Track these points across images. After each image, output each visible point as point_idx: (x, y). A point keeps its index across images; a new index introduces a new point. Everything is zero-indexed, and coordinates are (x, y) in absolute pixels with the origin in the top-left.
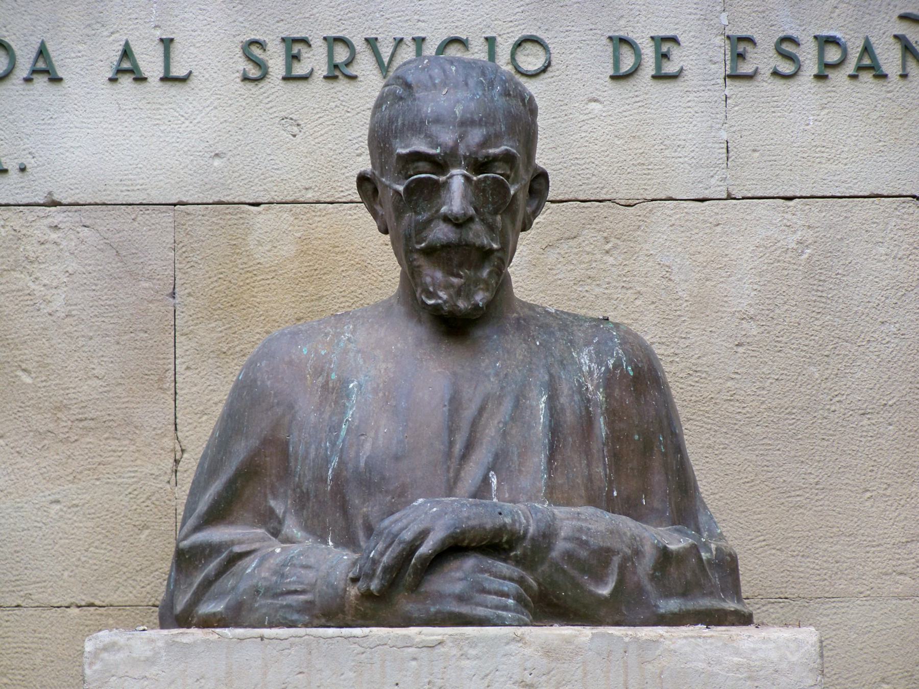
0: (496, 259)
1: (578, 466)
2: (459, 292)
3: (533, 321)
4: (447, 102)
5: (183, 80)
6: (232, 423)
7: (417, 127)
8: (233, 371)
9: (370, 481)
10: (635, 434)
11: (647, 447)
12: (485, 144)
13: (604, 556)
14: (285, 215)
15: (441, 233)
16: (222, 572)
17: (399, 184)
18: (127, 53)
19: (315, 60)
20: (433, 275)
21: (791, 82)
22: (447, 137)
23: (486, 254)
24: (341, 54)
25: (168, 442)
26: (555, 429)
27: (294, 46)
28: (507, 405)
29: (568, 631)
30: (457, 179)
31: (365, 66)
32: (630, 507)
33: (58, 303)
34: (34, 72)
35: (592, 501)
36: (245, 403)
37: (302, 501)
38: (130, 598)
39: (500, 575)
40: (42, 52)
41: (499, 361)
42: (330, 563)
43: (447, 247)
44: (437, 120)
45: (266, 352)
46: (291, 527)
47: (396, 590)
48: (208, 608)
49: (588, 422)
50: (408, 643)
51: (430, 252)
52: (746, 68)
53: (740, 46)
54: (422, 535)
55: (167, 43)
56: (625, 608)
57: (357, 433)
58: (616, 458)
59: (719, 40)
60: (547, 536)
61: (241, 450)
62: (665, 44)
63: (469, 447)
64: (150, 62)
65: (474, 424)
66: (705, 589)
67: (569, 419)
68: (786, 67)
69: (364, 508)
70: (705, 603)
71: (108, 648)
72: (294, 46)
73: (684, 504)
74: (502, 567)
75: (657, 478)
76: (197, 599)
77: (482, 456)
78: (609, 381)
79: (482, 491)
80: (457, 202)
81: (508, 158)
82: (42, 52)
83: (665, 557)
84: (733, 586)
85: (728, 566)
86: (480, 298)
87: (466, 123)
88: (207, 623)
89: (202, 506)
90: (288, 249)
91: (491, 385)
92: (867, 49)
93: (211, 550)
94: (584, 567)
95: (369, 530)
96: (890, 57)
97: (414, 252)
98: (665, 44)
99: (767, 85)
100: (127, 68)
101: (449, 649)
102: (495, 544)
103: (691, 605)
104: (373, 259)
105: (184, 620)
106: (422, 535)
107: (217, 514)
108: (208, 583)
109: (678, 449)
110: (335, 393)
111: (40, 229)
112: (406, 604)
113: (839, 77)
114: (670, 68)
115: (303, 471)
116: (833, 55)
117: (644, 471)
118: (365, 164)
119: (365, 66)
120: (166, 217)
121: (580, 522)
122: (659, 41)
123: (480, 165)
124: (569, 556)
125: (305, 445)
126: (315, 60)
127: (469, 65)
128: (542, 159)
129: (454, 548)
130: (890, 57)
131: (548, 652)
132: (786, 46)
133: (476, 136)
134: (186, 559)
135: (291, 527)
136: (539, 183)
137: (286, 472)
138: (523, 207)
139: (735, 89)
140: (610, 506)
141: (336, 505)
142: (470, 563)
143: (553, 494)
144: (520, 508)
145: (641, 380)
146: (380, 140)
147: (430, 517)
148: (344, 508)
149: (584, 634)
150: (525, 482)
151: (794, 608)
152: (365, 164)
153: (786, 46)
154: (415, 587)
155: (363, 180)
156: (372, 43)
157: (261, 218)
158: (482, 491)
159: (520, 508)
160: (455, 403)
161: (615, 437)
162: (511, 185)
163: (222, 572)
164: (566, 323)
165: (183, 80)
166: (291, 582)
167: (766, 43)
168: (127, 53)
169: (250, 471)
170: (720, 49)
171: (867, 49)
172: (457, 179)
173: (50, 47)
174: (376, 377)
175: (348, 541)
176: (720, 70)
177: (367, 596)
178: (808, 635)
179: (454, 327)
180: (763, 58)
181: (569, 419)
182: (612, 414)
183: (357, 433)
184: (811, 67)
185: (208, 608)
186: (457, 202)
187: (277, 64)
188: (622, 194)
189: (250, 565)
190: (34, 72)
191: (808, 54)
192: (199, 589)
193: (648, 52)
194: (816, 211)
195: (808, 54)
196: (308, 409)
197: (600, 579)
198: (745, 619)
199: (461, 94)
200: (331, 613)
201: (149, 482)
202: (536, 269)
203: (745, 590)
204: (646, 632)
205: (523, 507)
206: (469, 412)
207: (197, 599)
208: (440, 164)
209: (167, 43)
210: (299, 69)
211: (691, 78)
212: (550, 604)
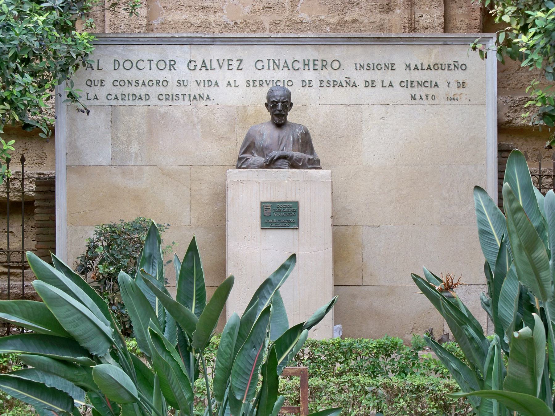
0: (285, 116)
1: (297, 146)
2: (280, 121)
3: (291, 125)
4: (278, 94)
6: (246, 139)
7: (274, 97)
8: (246, 131)
9: (267, 148)
10: (305, 142)
11: (307, 143)
12: (284, 99)
13: (300, 159)
14: (253, 107)
15: (277, 112)
16: (245, 161)
17: (271, 105)
18: (229, 82)
19: (257, 83)
20: (276, 118)
22: (278, 98)
23: (284, 115)
24: (261, 83)
26: (293, 141)
28: (287, 137)
29: (295, 170)
30: (280, 104)
31: (265, 84)
32: (304, 152)
33: (219, 120)
34: (202, 66)
35: (299, 151)
36: (248, 137)
37: (257, 151)
38: (229, 164)
39: (286, 162)
40: (216, 82)
41: (286, 131)
42: (261, 160)
43: (278, 114)
44: (277, 96)
45: (251, 129)
46: (255, 155)
47: (271, 164)
48: (243, 166)
49: (298, 140)
50: (273, 171)
51: (275, 115)
52: (322, 85)
53: (321, 82)
55: (235, 81)
56: (303, 167)
57: (265, 141)
58: (302, 145)
60: (292, 156)
61: (248, 144)
62: (310, 81)
63: (281, 143)
64: (232, 84)
65: (282, 140)
66: (314, 164)
67: (296, 139)
68: (328, 85)
69: (266, 152)
70: (315, 166)
71: (230, 172)
72: (254, 81)
73: (312, 151)
74: (286, 161)
75: (308, 148)
76: (242, 165)
77: (283, 145)
78: (301, 134)
79: (283, 150)
80: (279, 108)
81: (287, 101)
82: (216, 82)
83: (309, 159)
84: (319, 164)
85: (318, 161)
86: (283, 122)
87: (281, 96)
88: (243, 168)
89: (242, 151)
90: (253, 112)
91: (284, 134)
92: (341, 82)
93: (244, 158)
94: (298, 161)
95: (267, 155)
96: (344, 84)
97: (274, 115)
98: (310, 81)
99: (326, 88)
100: (229, 84)
101: (279, 173)
102: (285, 157)
103: (313, 166)
104: (267, 116)
105: (240, 168)
106: (274, 156)
107: (244, 152)
108: (243, 163)
109: (311, 143)
110: (262, 135)
111: (216, 109)
112: (273, 166)
113: (336, 87)
114: (311, 85)
115: (257, 147)
116: (335, 83)
117: (306, 147)
118: (266, 102)
119: (265, 84)
120: (235, 107)
121: (297, 154)
122: (309, 81)
123: (283, 102)
124: (296, 159)
125: (257, 143)
126: (257, 83)
127: (281, 87)
128: (291, 101)
129: (279, 158)
130: (344, 84)
131: (292, 173)
132: (328, 82)
133: (282, 98)
134: (240, 159)
135: (255, 155)
136: (291, 105)
137: (254, 147)
138: (289, 108)
139: (320, 88)
140: (301, 152)
141: (262, 151)
142: (281, 160)
143: (293, 150)
144: (289, 152)
145: (306, 134)
146: (268, 98)
147: (276, 153)
148: (263, 152)
149: (297, 170)
150: (289, 149)
151: (328, 166)
152: (266, 102)
153: (328, 82)
154: (274, 164)
155: (266, 104)
157: (249, 107)
158: (283, 150)
159: (289, 152)
160: (279, 137)
161: (302, 142)
162: (287, 105)
163: (245, 161)
164: (295, 125)
166: (256, 163)
167: (325, 81)
168: (229, 82)
169: (249, 146)
170: (318, 82)
171: (341, 82)
172: (280, 104)
174: (267, 133)
175: (264, 157)
176: (318, 85)
177: (267, 165)
178: (330, 171)
179: (279, 126)
180: (325, 84)
181: (296, 139)
182: (302, 138)
183: (265, 141)
184: (332, 85)
185: (243, 166)
186: (279, 108)
188: (303, 104)
189: (250, 160)
190: (202, 66)
191: (332, 83)
192: (242, 163)
193: (308, 82)
194: (333, 107)
195: (332, 83)
196: (258, 138)
197: (300, 163)
198: (321, 168)
199: (280, 92)
200: (262, 167)
201: (235, 147)
202: (291, 117)
203: (321, 164)
204: (306, 170)
205: (289, 151)
206: (281, 138)
207: (242, 165)
208: (277, 102)
209: (235, 81)
210: (255, 85)
211: (314, 86)
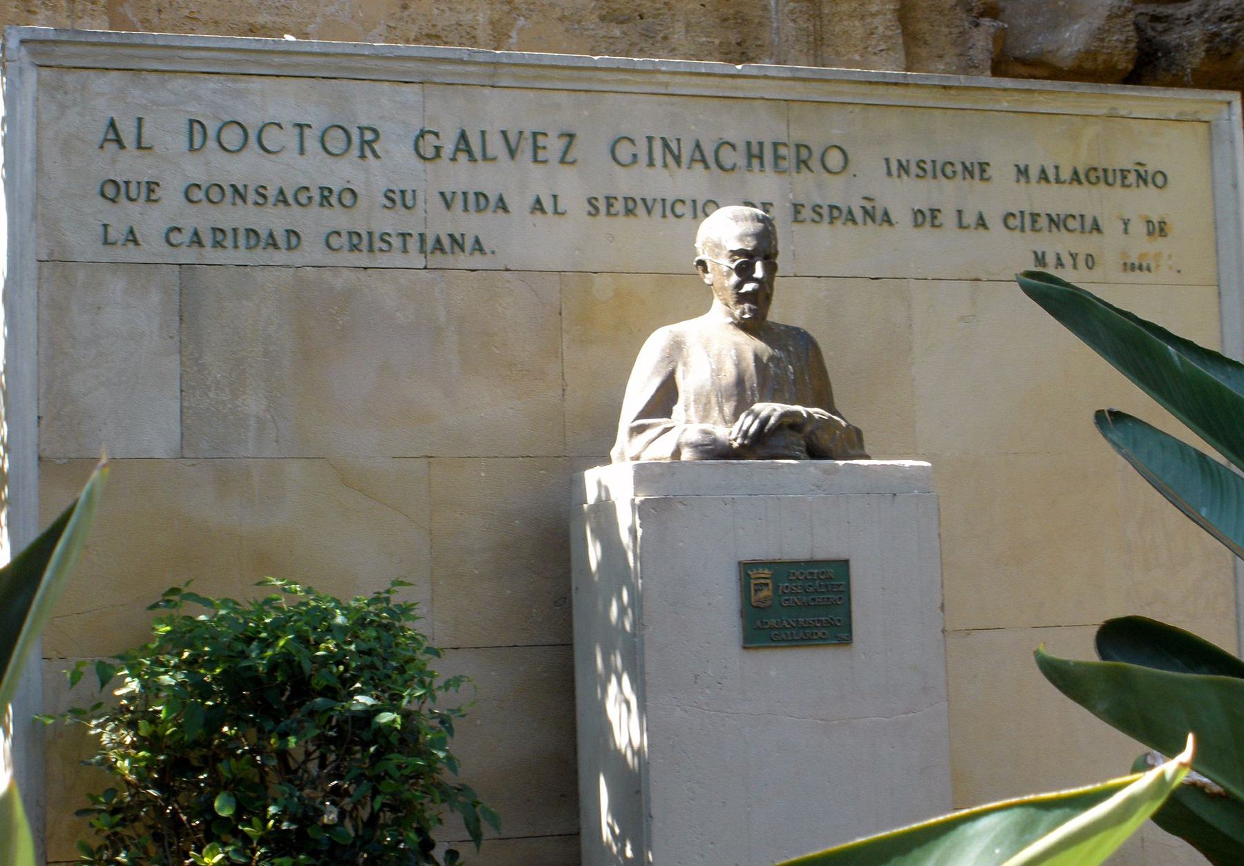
5: (563, 214)
19: (619, 206)
21: (303, 209)
25: (560, 382)
27: (610, 201)
39: (797, 440)
50: (43, 597)
54: (768, 418)
59: (788, 205)
64: (548, 204)
96: (858, 214)
99: (622, 220)
100: (538, 206)
113: (838, 223)
114: (153, 197)
126: (619, 206)
130: (858, 214)
156: (644, 200)
165: (563, 214)
173: (505, 197)
180: (807, 213)
187: (603, 208)
191: (825, 212)
212: (815, 452)
